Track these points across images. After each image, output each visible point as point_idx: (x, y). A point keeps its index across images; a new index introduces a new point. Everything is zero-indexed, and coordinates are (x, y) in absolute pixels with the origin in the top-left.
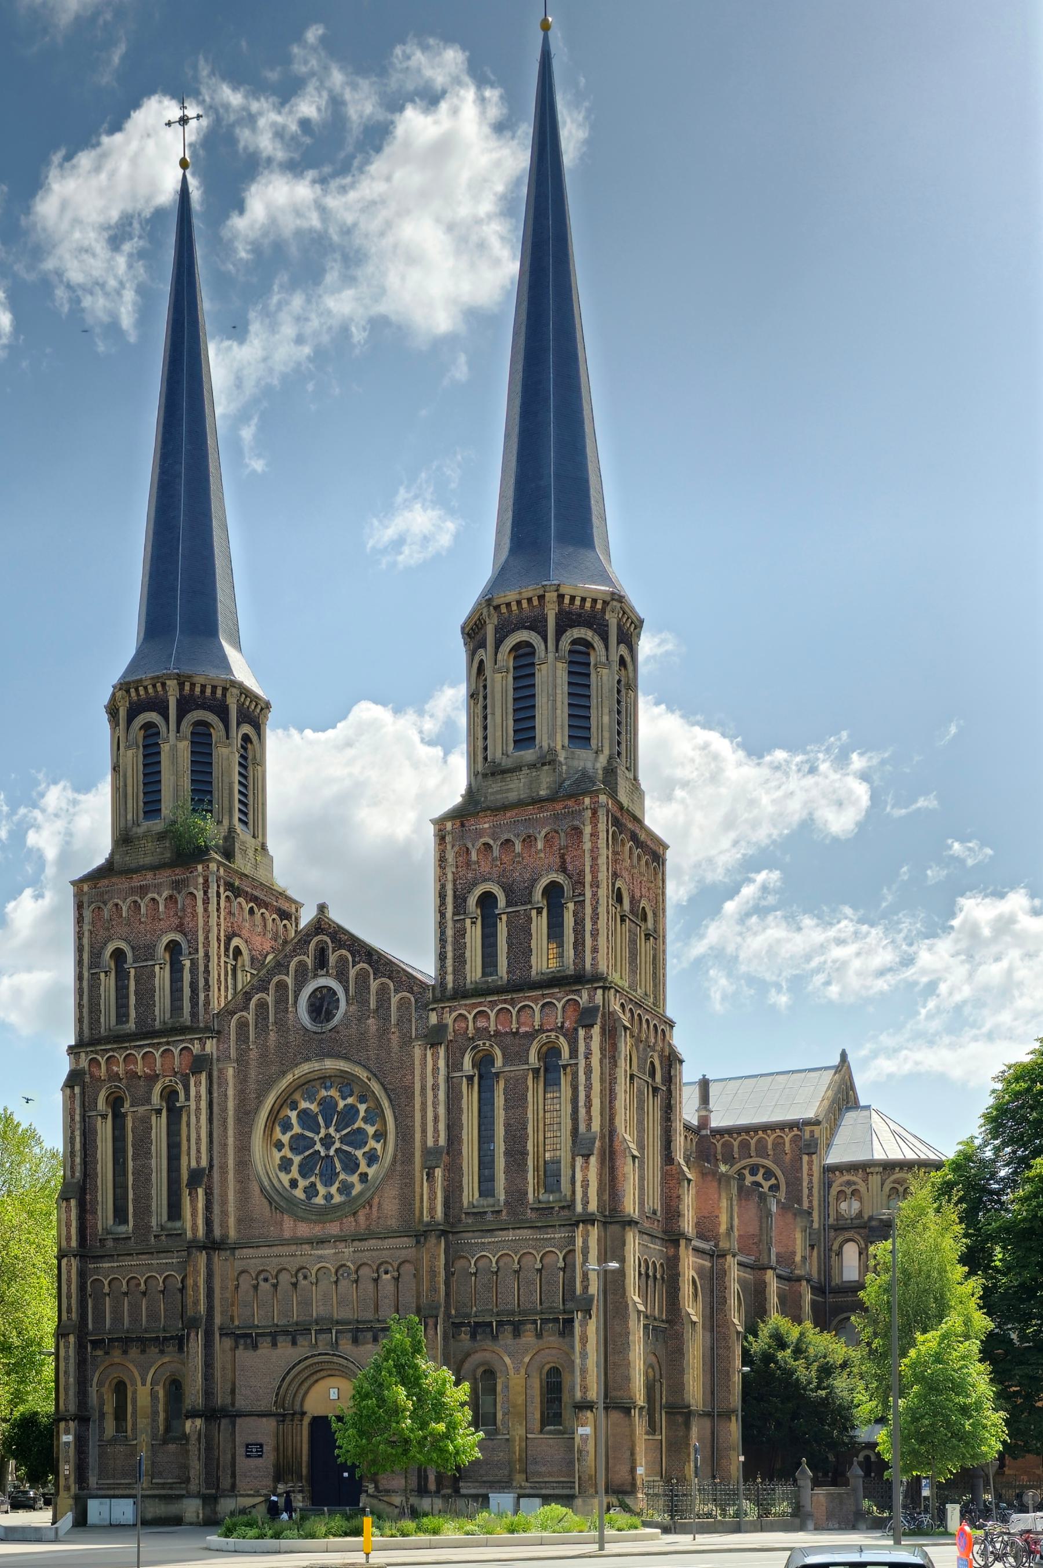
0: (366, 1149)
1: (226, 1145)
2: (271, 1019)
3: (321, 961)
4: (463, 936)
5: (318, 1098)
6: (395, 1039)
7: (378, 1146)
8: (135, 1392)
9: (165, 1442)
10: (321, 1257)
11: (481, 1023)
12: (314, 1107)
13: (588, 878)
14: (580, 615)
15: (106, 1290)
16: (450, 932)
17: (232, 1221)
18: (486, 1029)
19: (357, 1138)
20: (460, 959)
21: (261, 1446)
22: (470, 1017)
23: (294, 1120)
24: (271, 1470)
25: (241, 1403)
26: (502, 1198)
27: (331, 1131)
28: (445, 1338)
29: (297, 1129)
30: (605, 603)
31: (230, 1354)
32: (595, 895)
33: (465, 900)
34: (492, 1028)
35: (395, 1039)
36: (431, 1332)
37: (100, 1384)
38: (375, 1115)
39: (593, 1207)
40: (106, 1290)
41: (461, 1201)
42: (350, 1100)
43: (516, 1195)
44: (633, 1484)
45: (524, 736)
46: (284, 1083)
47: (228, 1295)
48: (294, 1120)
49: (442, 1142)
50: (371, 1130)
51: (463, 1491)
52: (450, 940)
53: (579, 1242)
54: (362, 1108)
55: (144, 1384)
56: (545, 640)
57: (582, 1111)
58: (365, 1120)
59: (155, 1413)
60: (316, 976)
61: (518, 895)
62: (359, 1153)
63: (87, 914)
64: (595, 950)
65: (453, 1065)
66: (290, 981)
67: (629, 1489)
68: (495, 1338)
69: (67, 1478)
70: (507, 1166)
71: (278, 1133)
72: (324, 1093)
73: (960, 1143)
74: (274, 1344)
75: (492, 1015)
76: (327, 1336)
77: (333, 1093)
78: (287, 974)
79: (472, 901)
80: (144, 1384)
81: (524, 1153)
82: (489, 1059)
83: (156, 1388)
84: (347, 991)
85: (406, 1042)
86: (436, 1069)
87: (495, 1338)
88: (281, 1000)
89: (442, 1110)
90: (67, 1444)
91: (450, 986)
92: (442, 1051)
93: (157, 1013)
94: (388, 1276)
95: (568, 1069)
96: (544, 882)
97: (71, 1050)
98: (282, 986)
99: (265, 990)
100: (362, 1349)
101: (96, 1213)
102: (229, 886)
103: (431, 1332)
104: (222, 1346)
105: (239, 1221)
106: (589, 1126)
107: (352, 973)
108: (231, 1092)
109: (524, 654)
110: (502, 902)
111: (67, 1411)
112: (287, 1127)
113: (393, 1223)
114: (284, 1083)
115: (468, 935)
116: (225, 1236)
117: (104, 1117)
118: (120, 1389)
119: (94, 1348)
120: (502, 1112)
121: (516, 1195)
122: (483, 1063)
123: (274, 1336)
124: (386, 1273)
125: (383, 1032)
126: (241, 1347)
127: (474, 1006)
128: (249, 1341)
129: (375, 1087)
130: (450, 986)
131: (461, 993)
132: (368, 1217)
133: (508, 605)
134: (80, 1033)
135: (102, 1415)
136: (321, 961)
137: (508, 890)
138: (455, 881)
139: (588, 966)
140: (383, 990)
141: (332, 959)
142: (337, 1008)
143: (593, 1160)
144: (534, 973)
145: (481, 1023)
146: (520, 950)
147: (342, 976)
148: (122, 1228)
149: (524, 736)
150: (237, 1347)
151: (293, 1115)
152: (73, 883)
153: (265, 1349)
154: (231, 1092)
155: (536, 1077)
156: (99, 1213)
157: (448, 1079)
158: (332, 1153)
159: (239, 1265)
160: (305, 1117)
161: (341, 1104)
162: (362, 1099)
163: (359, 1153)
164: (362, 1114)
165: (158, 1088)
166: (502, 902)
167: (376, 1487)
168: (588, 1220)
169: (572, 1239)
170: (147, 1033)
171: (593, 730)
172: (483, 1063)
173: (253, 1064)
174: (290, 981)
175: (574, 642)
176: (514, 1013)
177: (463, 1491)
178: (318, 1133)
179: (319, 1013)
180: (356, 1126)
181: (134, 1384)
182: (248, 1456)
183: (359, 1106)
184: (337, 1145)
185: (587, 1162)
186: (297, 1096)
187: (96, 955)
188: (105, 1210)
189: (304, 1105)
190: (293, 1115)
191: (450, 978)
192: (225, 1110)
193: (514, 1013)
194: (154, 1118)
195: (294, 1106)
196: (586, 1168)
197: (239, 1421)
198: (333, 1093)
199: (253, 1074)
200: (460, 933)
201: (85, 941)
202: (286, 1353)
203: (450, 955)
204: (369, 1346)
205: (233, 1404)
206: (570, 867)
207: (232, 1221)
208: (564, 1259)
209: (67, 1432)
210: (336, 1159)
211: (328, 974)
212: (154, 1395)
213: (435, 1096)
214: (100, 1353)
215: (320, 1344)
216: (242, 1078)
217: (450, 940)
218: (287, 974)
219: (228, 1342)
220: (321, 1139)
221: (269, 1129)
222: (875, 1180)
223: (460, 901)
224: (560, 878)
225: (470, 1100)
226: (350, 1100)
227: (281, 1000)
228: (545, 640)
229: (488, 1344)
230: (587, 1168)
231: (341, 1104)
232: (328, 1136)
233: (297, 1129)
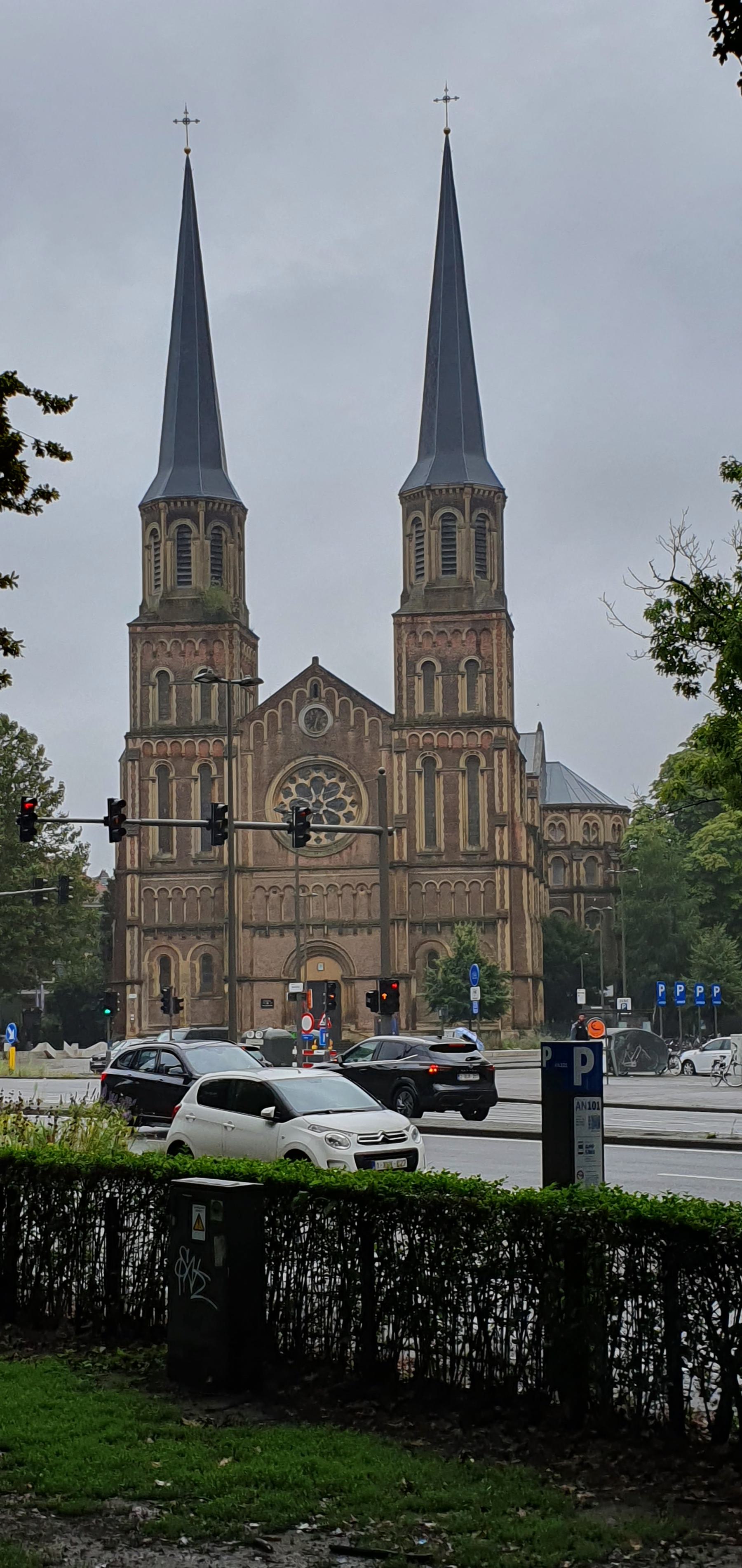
0: (345, 811)
1: (247, 804)
2: (280, 726)
3: (315, 692)
4: (413, 686)
5: (311, 777)
6: (367, 746)
7: (354, 810)
8: (178, 965)
9: (201, 998)
10: (316, 878)
11: (428, 740)
12: (307, 782)
13: (495, 660)
14: (481, 500)
15: (156, 896)
16: (404, 683)
17: (251, 854)
18: (432, 744)
19: (339, 804)
20: (411, 700)
21: (272, 1000)
22: (421, 737)
23: (293, 791)
24: (280, 1017)
25: (257, 973)
26: (443, 848)
27: (321, 799)
28: (410, 932)
29: (295, 796)
30: (496, 493)
31: (249, 940)
32: (500, 671)
33: (415, 665)
34: (436, 744)
35: (367, 746)
36: (401, 930)
37: (150, 959)
38: (353, 789)
39: (506, 857)
40: (156, 896)
41: (415, 847)
42: (333, 780)
43: (452, 846)
44: (530, 1024)
45: (449, 568)
46: (288, 768)
47: (247, 901)
48: (293, 791)
49: (405, 811)
50: (349, 799)
51: (418, 1029)
52: (405, 688)
53: (498, 878)
54: (342, 785)
55: (185, 959)
56: (464, 515)
57: (497, 799)
58: (344, 793)
59: (193, 979)
60: (310, 702)
61: (451, 668)
62: (340, 814)
63: (139, 646)
64: (500, 703)
65: (411, 765)
66: (293, 703)
67: (526, 1026)
68: (439, 933)
69: (132, 1023)
70: (445, 828)
71: (282, 798)
72: (315, 774)
73: (681, 745)
74: (282, 935)
75: (435, 736)
76: (321, 930)
77: (321, 774)
78: (291, 699)
79: (419, 669)
80: (185, 959)
81: (457, 821)
82: (433, 761)
83: (194, 962)
84: (333, 713)
85: (375, 748)
86: (400, 767)
87: (439, 933)
88: (287, 716)
89: (404, 793)
90: (133, 1000)
91: (405, 716)
92: (404, 756)
93: (193, 715)
94: (363, 893)
95: (485, 773)
96: (466, 659)
97: (127, 737)
98: (287, 706)
99: (276, 707)
100: (345, 938)
101: (148, 844)
102: (241, 636)
103: (401, 930)
104: (243, 935)
105: (256, 853)
106: (501, 808)
107: (338, 702)
108: (250, 770)
109: (449, 518)
110: (438, 669)
111: (132, 977)
112: (288, 793)
113: (367, 860)
114: (288, 768)
115: (416, 686)
116: (246, 863)
117: (154, 781)
118: (165, 963)
119: (145, 935)
120: (442, 796)
121: (452, 846)
122: (429, 762)
123: (282, 928)
124: (362, 890)
125: (359, 741)
126: (257, 936)
127: (424, 730)
128: (263, 932)
129: (353, 774)
130: (405, 716)
131: (414, 724)
132: (349, 855)
133: (440, 490)
134: (133, 724)
135: (152, 981)
136: (315, 692)
137: (443, 661)
138: (407, 653)
139: (496, 712)
140: (358, 714)
141: (323, 693)
142: (326, 723)
143: (506, 829)
144: (460, 713)
145: (428, 740)
146: (451, 698)
147: (330, 703)
148: (167, 856)
149: (449, 568)
150: (254, 936)
151: (293, 787)
152: (129, 625)
153: (275, 937)
154: (250, 770)
155: (464, 775)
156: (150, 845)
157: (408, 772)
158: (321, 812)
159: (256, 882)
160: (300, 787)
161: (327, 782)
162: (342, 779)
163: (340, 814)
164: (342, 789)
165: (196, 765)
166: (438, 669)
167: (357, 1027)
168: (503, 864)
169: (493, 875)
170: (191, 731)
171: (489, 566)
172: (429, 762)
173: (265, 753)
174: (293, 703)
175: (480, 515)
176: (450, 736)
177: (418, 1029)
178: (311, 799)
179: (313, 725)
180: (338, 796)
181: (177, 959)
182: (263, 1007)
183: (340, 784)
184: (325, 808)
185: (503, 829)
186: (296, 775)
187: (146, 673)
188: (153, 843)
189: (301, 781)
190: (293, 787)
191: (405, 711)
192: (245, 781)
193: (450, 736)
194: (193, 784)
195: (293, 780)
196: (501, 833)
197: (256, 984)
198: (321, 774)
199: (265, 760)
200: (411, 685)
201: (138, 664)
202: (289, 941)
203: (405, 697)
204: (351, 937)
205: (252, 973)
206: (483, 652)
207: (251, 854)
208: (484, 886)
209: (132, 992)
210: (323, 817)
211: (320, 701)
212: (193, 968)
213: (400, 783)
214: (149, 938)
215: (315, 934)
216: (258, 761)
217: (405, 688)
218: (291, 699)
219: (248, 933)
220: (313, 804)
221: (276, 795)
222: (575, 817)
223: (411, 665)
224: (476, 658)
225: (420, 785)
226: (333, 780)
227: (287, 716)
228: (464, 515)
229: (434, 937)
230: (502, 833)
231: (327, 782)
232: (318, 801)
233: (295, 796)
